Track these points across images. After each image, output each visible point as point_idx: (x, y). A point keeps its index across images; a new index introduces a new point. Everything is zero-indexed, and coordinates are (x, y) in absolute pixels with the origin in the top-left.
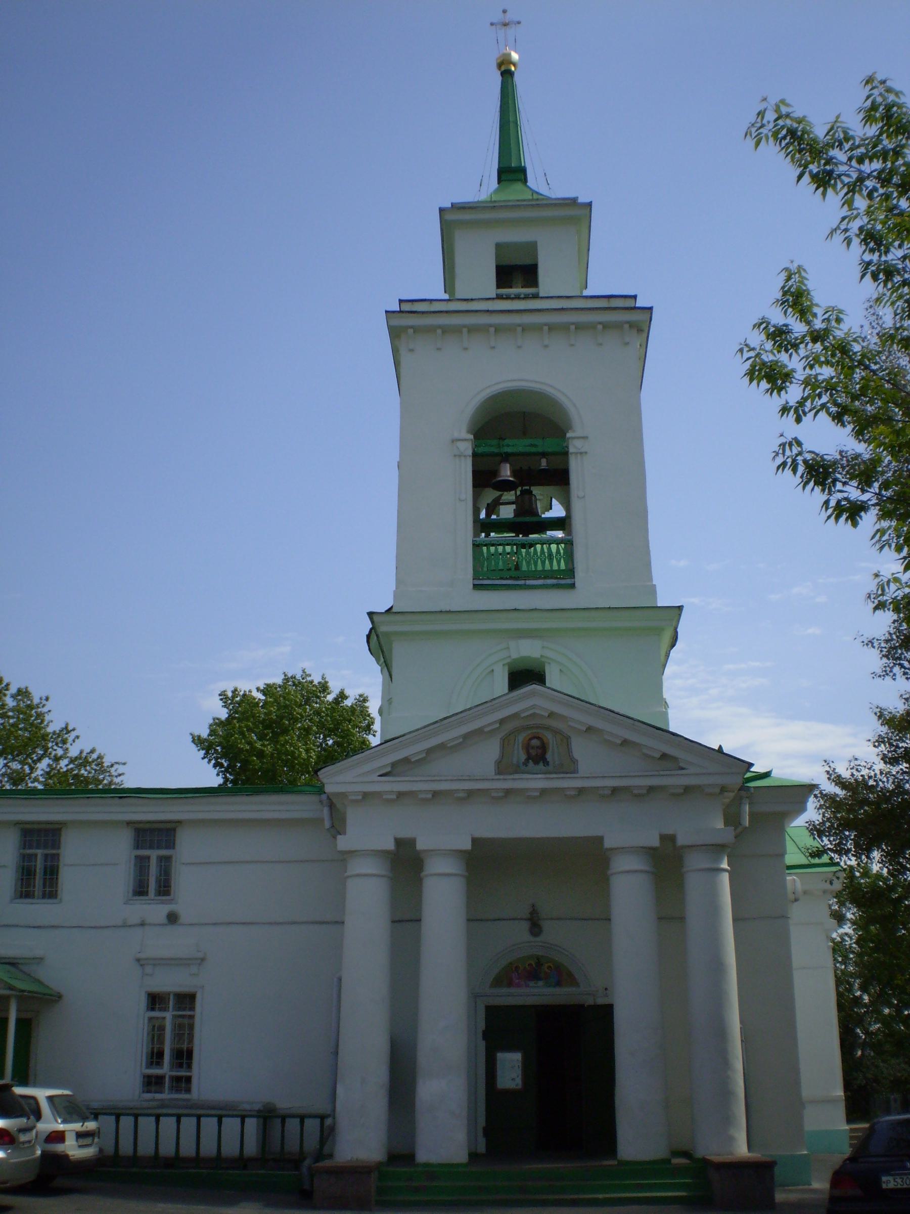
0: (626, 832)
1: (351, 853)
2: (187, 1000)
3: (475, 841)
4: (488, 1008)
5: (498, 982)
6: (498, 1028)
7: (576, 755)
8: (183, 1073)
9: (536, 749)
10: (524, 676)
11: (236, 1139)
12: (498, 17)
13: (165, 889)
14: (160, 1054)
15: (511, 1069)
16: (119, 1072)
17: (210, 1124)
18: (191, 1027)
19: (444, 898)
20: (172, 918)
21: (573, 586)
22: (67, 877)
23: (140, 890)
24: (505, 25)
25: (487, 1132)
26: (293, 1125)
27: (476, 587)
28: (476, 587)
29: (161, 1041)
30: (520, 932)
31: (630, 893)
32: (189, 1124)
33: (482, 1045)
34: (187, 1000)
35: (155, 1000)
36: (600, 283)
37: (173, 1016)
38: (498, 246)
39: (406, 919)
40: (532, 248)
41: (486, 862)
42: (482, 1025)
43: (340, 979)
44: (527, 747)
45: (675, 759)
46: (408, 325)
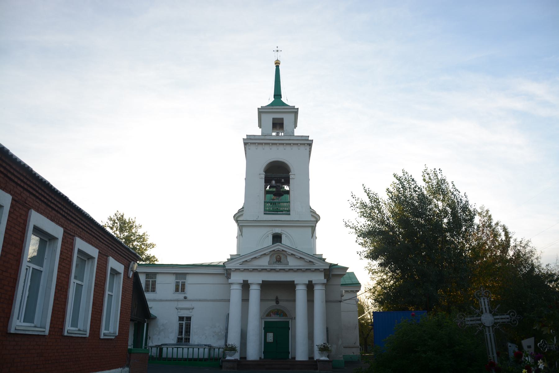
0: (301, 280)
1: (231, 283)
2: (189, 319)
3: (263, 281)
4: (265, 322)
5: (268, 315)
6: (268, 327)
7: (288, 260)
8: (188, 337)
9: (279, 257)
10: (277, 238)
11: (203, 353)
12: (276, 49)
13: (183, 290)
14: (182, 332)
15: (270, 337)
16: (171, 337)
17: (196, 350)
18: (190, 325)
19: (255, 294)
20: (185, 298)
21: (289, 214)
22: (158, 286)
23: (177, 290)
24: (277, 51)
25: (264, 353)
26: (217, 350)
27: (265, 214)
28: (265, 214)
29: (182, 328)
30: (274, 303)
31: (301, 294)
32: (191, 350)
33: (263, 331)
34: (189, 319)
35: (181, 319)
36: (298, 132)
37: (185, 325)
38: (273, 119)
39: (245, 299)
40: (282, 119)
41: (265, 286)
42: (263, 326)
43: (228, 314)
44: (276, 258)
45: (312, 262)
46: (249, 142)
